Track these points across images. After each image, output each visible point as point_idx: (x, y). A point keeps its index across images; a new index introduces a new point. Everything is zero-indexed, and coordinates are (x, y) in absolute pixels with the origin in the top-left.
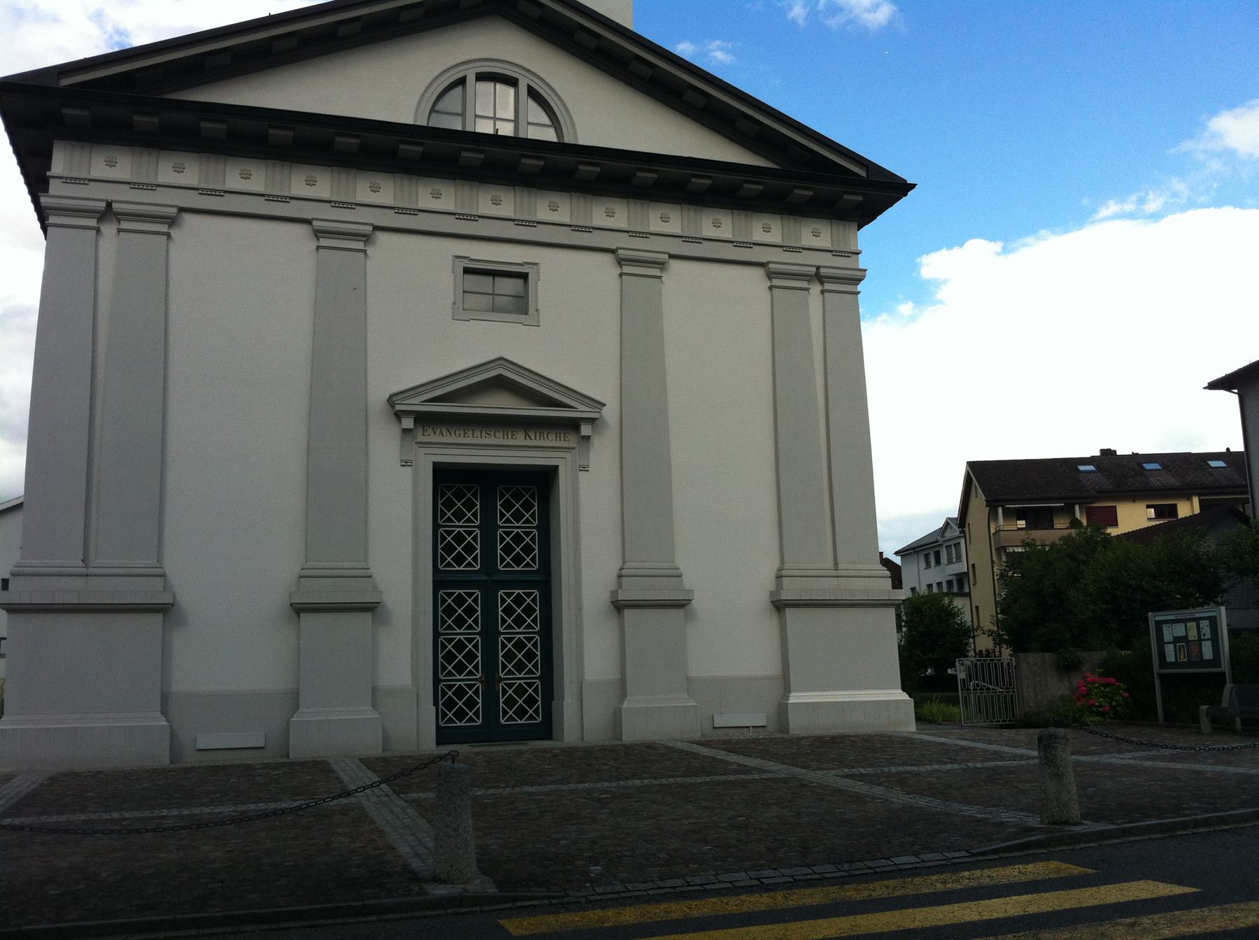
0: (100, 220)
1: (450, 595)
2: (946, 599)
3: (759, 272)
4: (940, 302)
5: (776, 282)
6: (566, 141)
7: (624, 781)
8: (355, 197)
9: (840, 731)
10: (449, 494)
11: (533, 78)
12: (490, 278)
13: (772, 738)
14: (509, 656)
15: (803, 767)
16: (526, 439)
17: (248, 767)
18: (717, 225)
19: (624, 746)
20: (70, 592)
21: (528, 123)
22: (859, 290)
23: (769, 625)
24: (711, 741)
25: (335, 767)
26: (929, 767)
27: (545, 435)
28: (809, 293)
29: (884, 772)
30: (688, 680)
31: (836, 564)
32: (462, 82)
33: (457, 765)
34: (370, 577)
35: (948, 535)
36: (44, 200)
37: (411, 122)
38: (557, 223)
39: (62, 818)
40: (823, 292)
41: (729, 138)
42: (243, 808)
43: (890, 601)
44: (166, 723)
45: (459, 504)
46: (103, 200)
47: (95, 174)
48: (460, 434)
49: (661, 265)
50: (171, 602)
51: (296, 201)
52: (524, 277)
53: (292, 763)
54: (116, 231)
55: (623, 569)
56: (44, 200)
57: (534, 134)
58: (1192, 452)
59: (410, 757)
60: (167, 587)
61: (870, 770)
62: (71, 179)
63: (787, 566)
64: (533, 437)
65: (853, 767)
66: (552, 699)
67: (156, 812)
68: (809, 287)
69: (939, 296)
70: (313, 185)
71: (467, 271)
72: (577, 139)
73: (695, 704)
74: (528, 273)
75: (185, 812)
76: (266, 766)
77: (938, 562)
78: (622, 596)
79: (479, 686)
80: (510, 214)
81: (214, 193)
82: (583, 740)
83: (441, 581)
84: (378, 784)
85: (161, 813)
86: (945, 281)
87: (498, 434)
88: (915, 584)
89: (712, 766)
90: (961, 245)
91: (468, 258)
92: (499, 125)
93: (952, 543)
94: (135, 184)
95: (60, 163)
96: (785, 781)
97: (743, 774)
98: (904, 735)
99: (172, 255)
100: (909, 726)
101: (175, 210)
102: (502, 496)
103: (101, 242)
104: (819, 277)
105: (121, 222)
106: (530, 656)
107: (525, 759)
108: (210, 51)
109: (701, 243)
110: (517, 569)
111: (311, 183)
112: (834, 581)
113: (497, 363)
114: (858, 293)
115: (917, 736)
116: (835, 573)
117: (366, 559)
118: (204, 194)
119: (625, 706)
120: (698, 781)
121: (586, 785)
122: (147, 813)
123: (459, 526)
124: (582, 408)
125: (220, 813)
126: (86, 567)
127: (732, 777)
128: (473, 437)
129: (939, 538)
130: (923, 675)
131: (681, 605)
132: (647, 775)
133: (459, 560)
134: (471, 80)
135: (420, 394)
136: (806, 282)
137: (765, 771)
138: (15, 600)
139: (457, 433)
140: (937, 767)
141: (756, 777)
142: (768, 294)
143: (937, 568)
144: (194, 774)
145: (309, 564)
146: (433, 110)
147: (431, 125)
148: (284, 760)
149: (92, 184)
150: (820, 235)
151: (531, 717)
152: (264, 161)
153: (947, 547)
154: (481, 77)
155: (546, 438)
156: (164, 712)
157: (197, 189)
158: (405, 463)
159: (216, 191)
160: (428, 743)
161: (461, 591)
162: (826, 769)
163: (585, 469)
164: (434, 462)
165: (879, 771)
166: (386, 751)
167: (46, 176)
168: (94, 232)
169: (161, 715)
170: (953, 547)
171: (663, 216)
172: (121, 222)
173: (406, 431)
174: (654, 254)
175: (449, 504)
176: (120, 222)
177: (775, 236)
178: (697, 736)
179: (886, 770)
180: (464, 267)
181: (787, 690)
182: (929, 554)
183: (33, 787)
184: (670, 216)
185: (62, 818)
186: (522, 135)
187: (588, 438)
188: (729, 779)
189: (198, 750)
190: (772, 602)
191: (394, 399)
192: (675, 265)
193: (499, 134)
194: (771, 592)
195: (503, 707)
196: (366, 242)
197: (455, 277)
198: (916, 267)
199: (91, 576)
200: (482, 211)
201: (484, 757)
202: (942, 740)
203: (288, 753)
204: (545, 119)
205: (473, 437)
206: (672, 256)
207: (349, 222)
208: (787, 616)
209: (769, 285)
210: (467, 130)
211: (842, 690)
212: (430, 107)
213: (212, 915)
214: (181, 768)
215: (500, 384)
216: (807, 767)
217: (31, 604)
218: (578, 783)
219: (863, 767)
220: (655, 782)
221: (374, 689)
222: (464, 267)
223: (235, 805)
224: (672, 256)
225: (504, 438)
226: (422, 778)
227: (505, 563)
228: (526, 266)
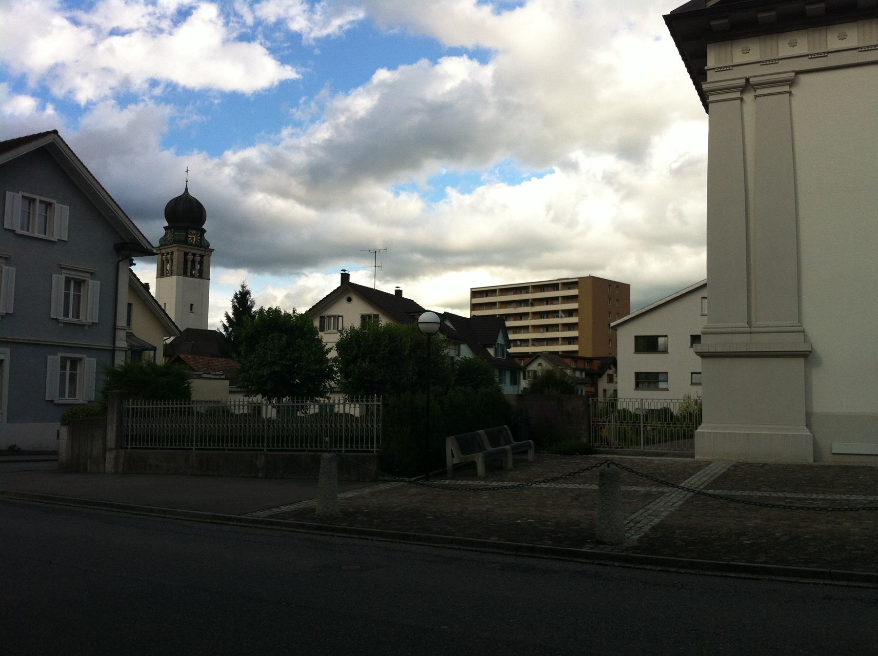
0: (742, 92)
8: (827, 48)
20: (740, 343)
39: (746, 493)
42: (871, 498)
44: (809, 434)
46: (742, 78)
47: (736, 61)
50: (810, 350)
54: (754, 96)
56: (705, 87)
58: (692, 82)
60: (806, 339)
67: (808, 495)
70: (844, 38)
75: (829, 497)
85: (812, 496)
94: (763, 62)
95: (713, 59)
99: (793, 105)
101: (793, 74)
105: (757, 90)
112: (745, 338)
116: (748, 330)
118: (819, 57)
122: (802, 496)
125: (855, 500)
126: (750, 327)
138: (705, 350)
144: (831, 470)
152: (856, 22)
156: (809, 426)
157: (807, 55)
167: (705, 70)
168: (739, 101)
169: (806, 428)
183: (724, 470)
185: (746, 493)
189: (834, 454)
207: (726, 80)
213: (857, 573)
217: (716, 352)
223: (865, 495)
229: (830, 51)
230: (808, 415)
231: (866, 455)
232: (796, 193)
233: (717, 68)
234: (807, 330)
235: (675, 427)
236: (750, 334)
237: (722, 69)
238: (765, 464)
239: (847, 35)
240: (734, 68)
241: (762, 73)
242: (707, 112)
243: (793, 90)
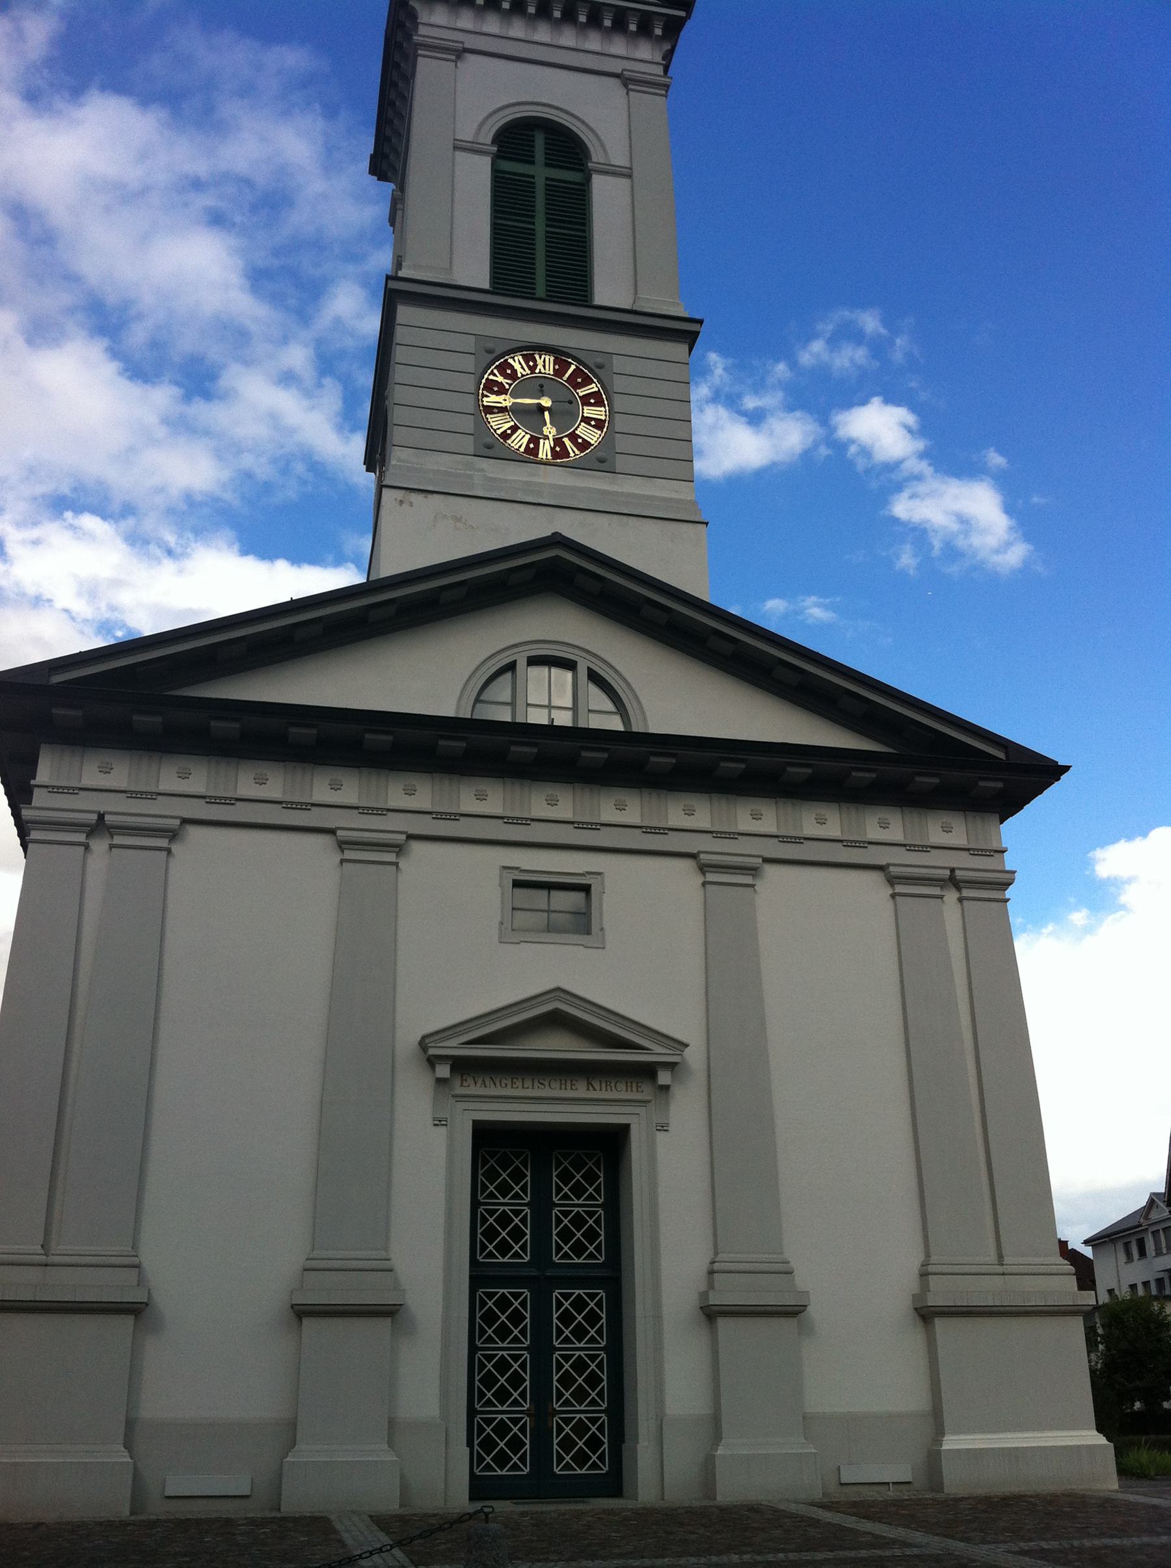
1: (490, 1296)
2: (1155, 1303)
3: (875, 877)
4: (1123, 907)
5: (899, 889)
6: (635, 729)
7: (717, 1556)
8: (158, 787)
9: (1015, 1489)
10: (492, 1162)
11: (593, 660)
12: (545, 892)
13: (919, 1499)
14: (566, 1380)
15: (962, 1540)
16: (588, 1089)
17: (228, 1522)
18: (884, 825)
19: (718, 1507)
21: (589, 710)
22: (1007, 897)
23: (913, 1339)
24: (837, 1502)
25: (339, 1527)
26: (1136, 1540)
27: (613, 1085)
28: (943, 901)
29: (1073, 1547)
30: (804, 1417)
31: (1000, 1257)
32: (511, 667)
33: (492, 1526)
34: (391, 1270)
35: (1155, 1216)
36: (26, 813)
37: (451, 714)
38: (474, 813)
40: (961, 900)
41: (831, 719)
43: (1075, 1308)
45: (504, 1175)
47: (86, 782)
48: (506, 1084)
49: (753, 871)
50: (146, 1301)
52: (586, 889)
53: (284, 1519)
54: (108, 846)
55: (714, 1262)
56: (26, 813)
57: (595, 723)
58: (7, 802)
59: (434, 1515)
60: (141, 1281)
61: (1054, 1544)
62: (58, 788)
63: (934, 1259)
64: (597, 1087)
65: (1031, 1540)
66: (623, 1441)
68: (943, 894)
69: (1123, 899)
70: (107, 772)
71: (517, 884)
72: (646, 725)
73: (814, 1451)
76: (252, 1522)
77: (1143, 1253)
78: (714, 1300)
79: (526, 1421)
80: (569, 816)
82: (663, 1499)
83: (480, 1277)
84: (389, 1547)
86: (1130, 881)
87: (553, 1084)
88: (1113, 1285)
89: (838, 1537)
90: (1145, 834)
92: (555, 714)
93: (1159, 1227)
94: (132, 792)
96: (937, 1559)
97: (880, 1548)
98: (1101, 1494)
100: (1109, 1482)
101: (178, 822)
102: (559, 1164)
103: (89, 861)
104: (953, 881)
105: (345, 851)
106: (593, 1380)
107: (584, 1522)
108: (149, 660)
109: (736, 838)
110: (577, 1261)
111: (336, 787)
112: (32, 1275)
113: (552, 995)
114: (1008, 900)
115: (1121, 1496)
116: (999, 1269)
117: (386, 1248)
119: (719, 1452)
120: (818, 1558)
121: (666, 1560)
123: (504, 1203)
126: (46, 1255)
127: (863, 1553)
128: (523, 1087)
129: (1142, 1220)
130: (1129, 1411)
131: (794, 1312)
132: (749, 1549)
133: (504, 1248)
134: (522, 664)
135: (458, 1034)
136: (939, 888)
137: (910, 1545)
140: (1146, 1539)
141: (898, 1552)
142: (890, 904)
143: (1142, 1262)
145: (316, 1254)
146: (477, 700)
147: (474, 717)
148: (274, 1514)
149: (82, 793)
150: (695, 813)
151: (594, 1466)
153: (1153, 1232)
154: (534, 661)
155: (613, 1088)
156: (128, 1445)
157: (280, 803)
158: (439, 1122)
159: (226, 798)
160: (459, 1499)
161: (505, 1291)
162: (994, 1543)
163: (663, 1128)
164: (473, 1121)
165: (1067, 1546)
166: (405, 1506)
169: (123, 1449)
170: (1161, 1232)
171: (944, 825)
173: (440, 1082)
175: (492, 1175)
176: (112, 837)
177: (895, 832)
178: (818, 1495)
179: (1076, 1543)
180: (513, 880)
181: (939, 1432)
182: (1130, 1242)
184: (953, 825)
186: (582, 724)
187: (666, 1088)
188: (860, 1555)
189: (168, 1497)
190: (916, 1309)
191: (427, 1041)
192: (771, 871)
193: (554, 724)
194: (913, 1295)
195: (557, 1450)
196: (398, 854)
197: (503, 894)
198: (1089, 864)
200: (535, 813)
201: (532, 1518)
202: (1155, 1501)
203: (279, 1505)
204: (609, 706)
205: (523, 1087)
206: (767, 860)
208: (936, 1327)
209: (891, 892)
210: (517, 721)
212: (474, 698)
214: (144, 1521)
215: (556, 1021)
216: (967, 1540)
218: (655, 1558)
219: (1045, 1540)
220: (759, 1558)
221: (392, 1423)
222: (513, 880)
224: (767, 860)
225: (561, 1089)
226: (449, 1545)
227: (562, 1253)
228: (589, 877)
229: (315, 802)
230: (130, 1424)
231: (235, 1497)
232: (156, 1019)
233: (53, 787)
234: (146, 1264)
236: (44, 1268)
237: (228, 801)
238: (40, 1524)
239: (267, 779)
240: (81, 793)
242: (25, 857)
243: (175, 848)
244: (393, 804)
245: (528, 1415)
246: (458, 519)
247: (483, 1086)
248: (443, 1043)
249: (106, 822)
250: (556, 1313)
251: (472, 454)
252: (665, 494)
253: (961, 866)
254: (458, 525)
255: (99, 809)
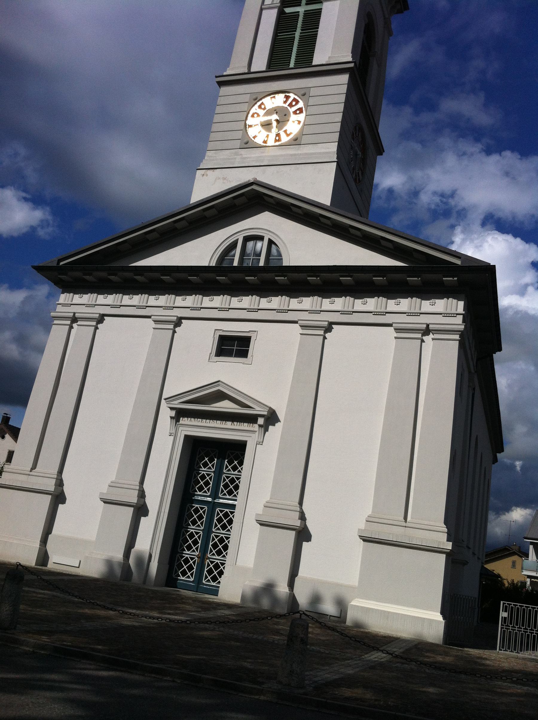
38: (181, 306)
46: (72, 313)
51: (73, 306)
74: (251, 336)
81: (313, 312)
91: (221, 330)
105: (434, 334)
116: (404, 524)
124: (257, 408)
139: (198, 421)
145: (273, 501)
172: (434, 334)
174: (318, 322)
199: (407, 527)
207: (69, 312)
211: (382, 602)
235: (508, 629)
236: (405, 528)
241: (66, 311)
244: (75, 302)
245: (197, 557)
246: (224, 179)
247: (190, 421)
248: (173, 402)
249: (430, 328)
250: (216, 517)
251: (239, 148)
252: (323, 151)
253: (78, 312)
254: (225, 181)
255: (426, 322)
